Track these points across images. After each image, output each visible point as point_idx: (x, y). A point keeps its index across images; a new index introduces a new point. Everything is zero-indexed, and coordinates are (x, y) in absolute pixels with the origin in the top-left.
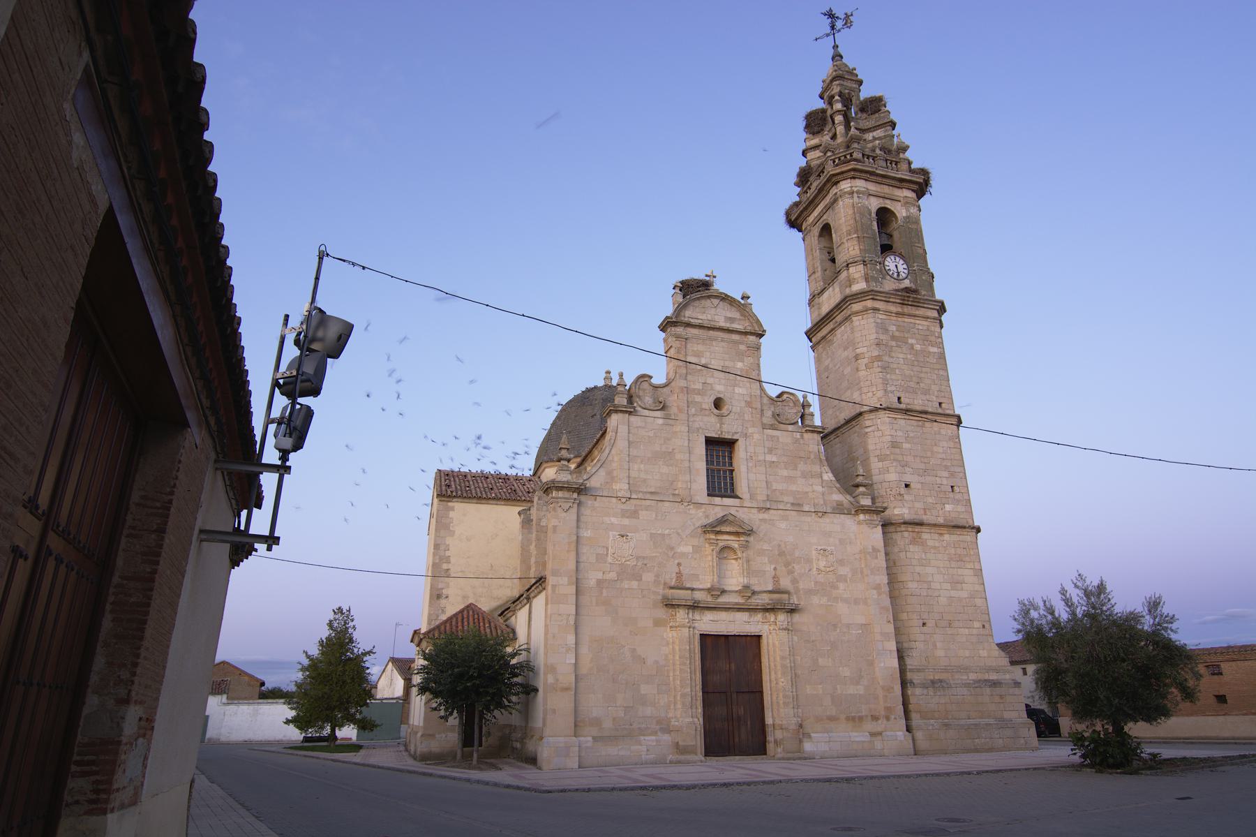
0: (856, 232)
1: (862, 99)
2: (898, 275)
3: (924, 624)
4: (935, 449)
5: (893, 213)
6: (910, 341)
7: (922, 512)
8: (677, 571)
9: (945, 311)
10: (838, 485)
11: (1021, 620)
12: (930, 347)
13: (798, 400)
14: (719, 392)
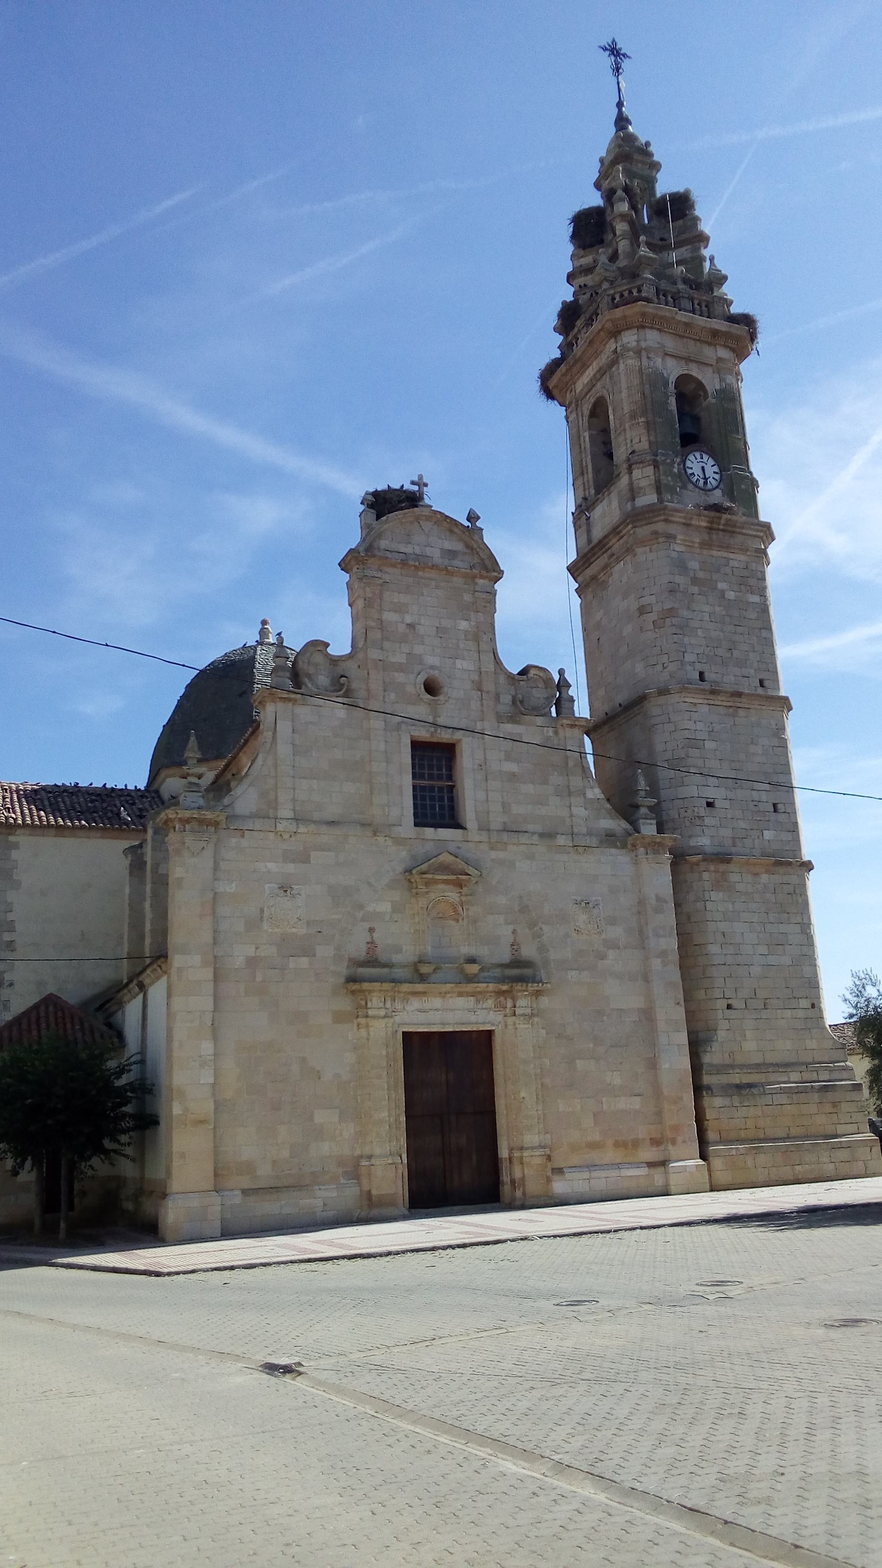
0: (644, 413)
1: (658, 194)
2: (705, 483)
5: (700, 385)
6: (721, 586)
7: (730, 842)
8: (369, 940)
9: (773, 539)
10: (608, 806)
11: (854, 1000)
12: (750, 596)
13: (552, 679)
14: (432, 667)
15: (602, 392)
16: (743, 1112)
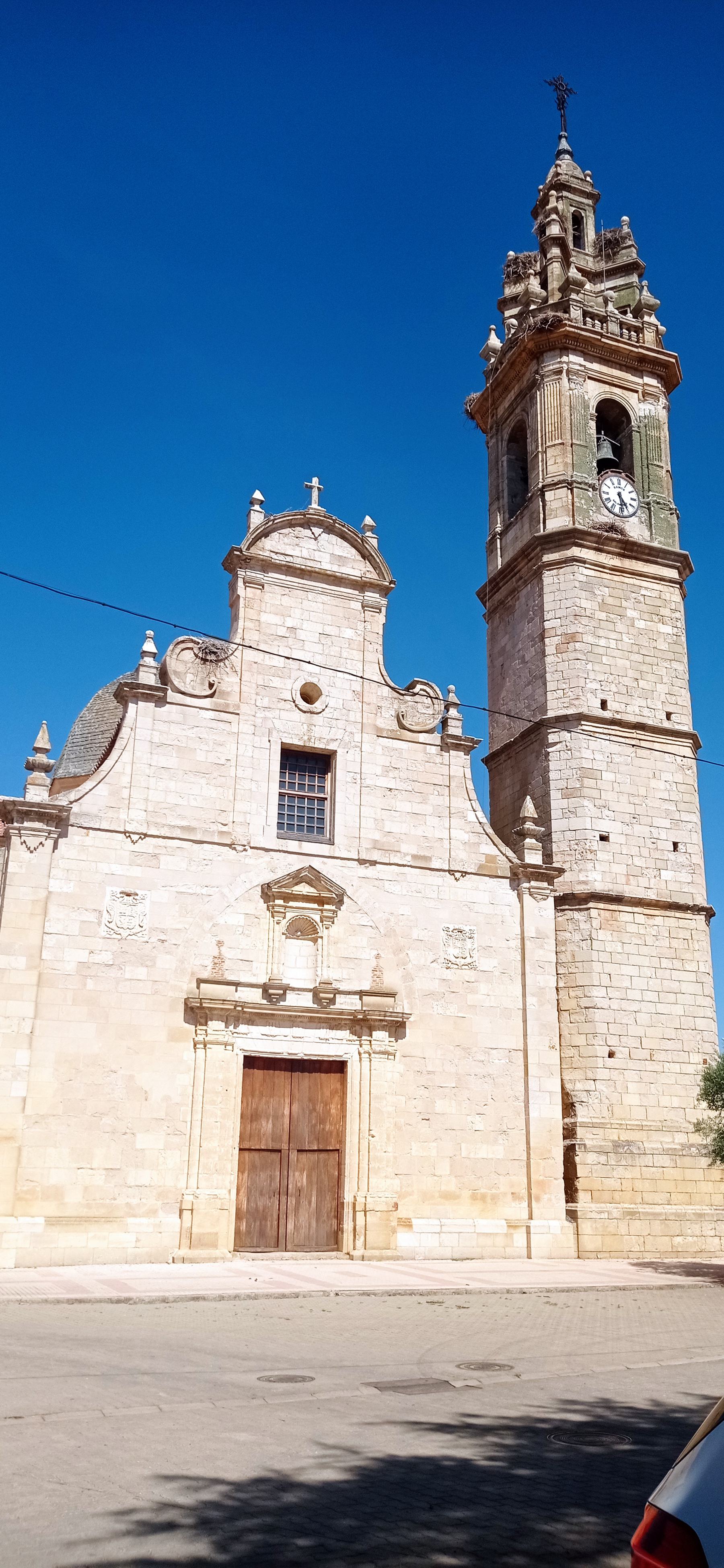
3: (611, 1055)
4: (654, 783)
7: (623, 880)
8: (216, 954)
12: (660, 625)
15: (522, 415)
16: (620, 1172)
